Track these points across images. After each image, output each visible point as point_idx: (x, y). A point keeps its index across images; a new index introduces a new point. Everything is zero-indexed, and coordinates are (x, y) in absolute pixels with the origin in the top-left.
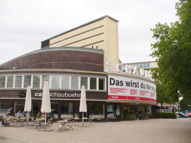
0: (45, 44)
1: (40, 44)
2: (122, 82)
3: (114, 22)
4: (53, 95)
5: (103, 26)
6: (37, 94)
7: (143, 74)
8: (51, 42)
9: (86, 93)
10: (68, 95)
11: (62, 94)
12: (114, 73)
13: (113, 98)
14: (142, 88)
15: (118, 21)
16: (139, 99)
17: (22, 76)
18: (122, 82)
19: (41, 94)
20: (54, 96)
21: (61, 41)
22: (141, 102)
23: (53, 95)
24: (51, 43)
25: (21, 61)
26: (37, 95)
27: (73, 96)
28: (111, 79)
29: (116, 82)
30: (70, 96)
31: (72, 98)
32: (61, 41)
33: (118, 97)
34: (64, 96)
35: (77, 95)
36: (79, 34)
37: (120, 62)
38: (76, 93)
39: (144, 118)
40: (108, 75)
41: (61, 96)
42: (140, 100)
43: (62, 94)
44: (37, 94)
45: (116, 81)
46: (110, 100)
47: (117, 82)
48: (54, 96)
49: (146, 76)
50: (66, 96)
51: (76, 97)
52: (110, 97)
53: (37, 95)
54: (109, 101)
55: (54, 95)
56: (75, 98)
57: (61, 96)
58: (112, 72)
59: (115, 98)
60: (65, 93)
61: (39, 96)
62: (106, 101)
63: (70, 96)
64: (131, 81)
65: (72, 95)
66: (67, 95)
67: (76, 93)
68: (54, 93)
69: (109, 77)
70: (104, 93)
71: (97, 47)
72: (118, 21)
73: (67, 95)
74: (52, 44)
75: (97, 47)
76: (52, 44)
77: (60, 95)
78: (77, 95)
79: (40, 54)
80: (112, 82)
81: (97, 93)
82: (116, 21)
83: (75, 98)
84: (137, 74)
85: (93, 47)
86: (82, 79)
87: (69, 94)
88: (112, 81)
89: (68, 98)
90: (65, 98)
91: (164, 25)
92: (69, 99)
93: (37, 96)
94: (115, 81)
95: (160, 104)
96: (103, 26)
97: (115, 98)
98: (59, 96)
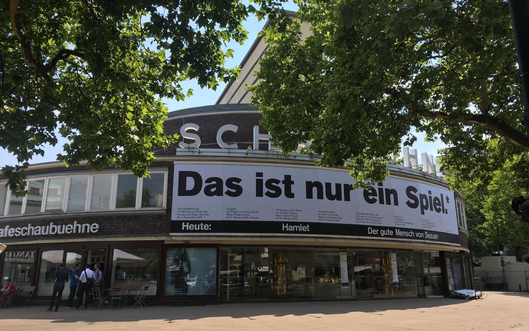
1: (519, 263)
2: (413, 202)
4: (25, 231)
10: (58, 228)
13: (189, 231)
14: (394, 192)
17: (117, 206)
18: (413, 202)
20: (71, 231)
22: (249, 239)
28: (183, 175)
29: (204, 185)
31: (65, 236)
33: (436, 237)
34: (198, 229)
35: (77, 227)
40: (175, 162)
41: (41, 232)
42: (101, 232)
45: (209, 180)
46: (177, 237)
47: (371, 197)
48: (71, 231)
50: (51, 233)
51: (74, 232)
52: (177, 226)
54: (174, 238)
56: (72, 236)
57: (41, 232)
59: (194, 231)
60: (51, 223)
62: (163, 241)
64: (430, 192)
66: (54, 229)
68: (27, 227)
69: (179, 167)
70: (158, 217)
73: (54, 229)
77: (39, 230)
78: (77, 227)
80: (190, 183)
81: (136, 217)
83: (72, 236)
88: (190, 183)
89: (57, 236)
90: (48, 237)
93: (12, 235)
94: (204, 180)
95: (303, 275)
97: (194, 231)
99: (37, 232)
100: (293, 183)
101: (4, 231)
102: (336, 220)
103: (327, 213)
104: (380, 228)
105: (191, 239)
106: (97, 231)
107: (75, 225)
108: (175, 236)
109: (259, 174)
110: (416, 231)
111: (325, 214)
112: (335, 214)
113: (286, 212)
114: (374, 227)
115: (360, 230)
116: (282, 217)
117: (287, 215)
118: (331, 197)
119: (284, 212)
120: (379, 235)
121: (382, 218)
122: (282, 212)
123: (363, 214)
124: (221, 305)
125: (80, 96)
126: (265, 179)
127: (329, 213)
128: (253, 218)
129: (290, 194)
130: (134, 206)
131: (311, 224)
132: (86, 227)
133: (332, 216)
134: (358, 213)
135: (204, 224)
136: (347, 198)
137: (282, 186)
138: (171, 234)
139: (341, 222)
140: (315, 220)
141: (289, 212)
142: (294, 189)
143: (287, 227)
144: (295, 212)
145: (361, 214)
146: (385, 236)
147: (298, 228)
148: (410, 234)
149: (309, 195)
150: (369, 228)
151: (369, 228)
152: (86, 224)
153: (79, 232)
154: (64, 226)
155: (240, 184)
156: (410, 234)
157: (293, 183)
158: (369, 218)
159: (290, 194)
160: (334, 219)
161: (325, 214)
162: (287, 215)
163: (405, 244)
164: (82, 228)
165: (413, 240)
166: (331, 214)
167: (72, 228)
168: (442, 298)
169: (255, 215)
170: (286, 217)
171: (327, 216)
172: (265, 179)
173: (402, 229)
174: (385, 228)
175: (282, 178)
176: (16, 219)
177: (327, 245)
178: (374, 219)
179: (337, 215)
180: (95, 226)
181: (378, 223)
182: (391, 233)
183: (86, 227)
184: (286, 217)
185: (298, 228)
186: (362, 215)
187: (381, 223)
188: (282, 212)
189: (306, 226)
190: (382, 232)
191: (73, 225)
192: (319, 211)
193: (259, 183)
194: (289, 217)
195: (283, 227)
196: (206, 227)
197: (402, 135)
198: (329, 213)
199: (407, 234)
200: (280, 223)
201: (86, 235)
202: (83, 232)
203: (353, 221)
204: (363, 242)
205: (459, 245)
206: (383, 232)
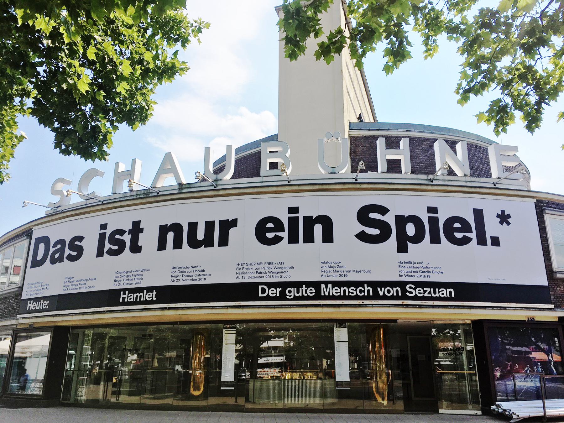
11: (138, 300)
20: (363, 294)
27: (337, 293)
33: (44, 304)
38: (366, 285)
43: (138, 300)
48: (363, 294)
51: (342, 294)
54: (21, 321)
55: (364, 291)
80: (411, 229)
88: (411, 229)
98: (443, 294)
99: (130, 299)
100: (142, 231)
102: (200, 279)
103: (187, 270)
104: (284, 285)
106: (314, 294)
107: (366, 289)
108: (23, 318)
109: (293, 210)
110: (374, 285)
111: (182, 272)
112: (200, 269)
113: (129, 274)
114: (270, 285)
115: (245, 292)
116: (122, 282)
117: (129, 278)
118: (194, 243)
119: (125, 274)
120: (282, 296)
121: (292, 267)
122: (123, 274)
123: (251, 264)
124: (79, 409)
126: (301, 216)
127: (190, 269)
128: (89, 287)
129: (136, 248)
131: (158, 289)
133: (194, 273)
134: (241, 264)
135: (307, 287)
136: (224, 242)
137: (127, 238)
138: (19, 316)
139: (209, 281)
140: (166, 281)
141: (131, 274)
142: (142, 240)
143: (126, 296)
144: (140, 273)
145: (248, 264)
146: (295, 298)
147: (141, 296)
148: (361, 291)
149: (162, 246)
150: (260, 287)
151: (260, 287)
155: (361, 228)
156: (361, 291)
157: (142, 231)
158: (263, 270)
159: (136, 248)
160: (197, 278)
161: (182, 272)
162: (129, 278)
163: (342, 309)
165: (366, 302)
166: (192, 269)
168: (476, 415)
169: (89, 283)
170: (127, 282)
171: (185, 274)
172: (108, 231)
173: (418, 284)
174: (298, 285)
175: (128, 227)
177: (184, 319)
178: (273, 270)
179: (344, 267)
180: (311, 290)
181: (282, 277)
182: (311, 292)
184: (127, 282)
185: (141, 296)
186: (250, 266)
187: (290, 277)
188: (123, 274)
189: (152, 292)
190: (290, 292)
192: (174, 268)
193: (102, 237)
194: (131, 282)
195: (122, 296)
196: (44, 304)
198: (190, 269)
199: (353, 291)
200: (116, 293)
203: (230, 278)
204: (246, 311)
205: (552, 306)
206: (292, 292)
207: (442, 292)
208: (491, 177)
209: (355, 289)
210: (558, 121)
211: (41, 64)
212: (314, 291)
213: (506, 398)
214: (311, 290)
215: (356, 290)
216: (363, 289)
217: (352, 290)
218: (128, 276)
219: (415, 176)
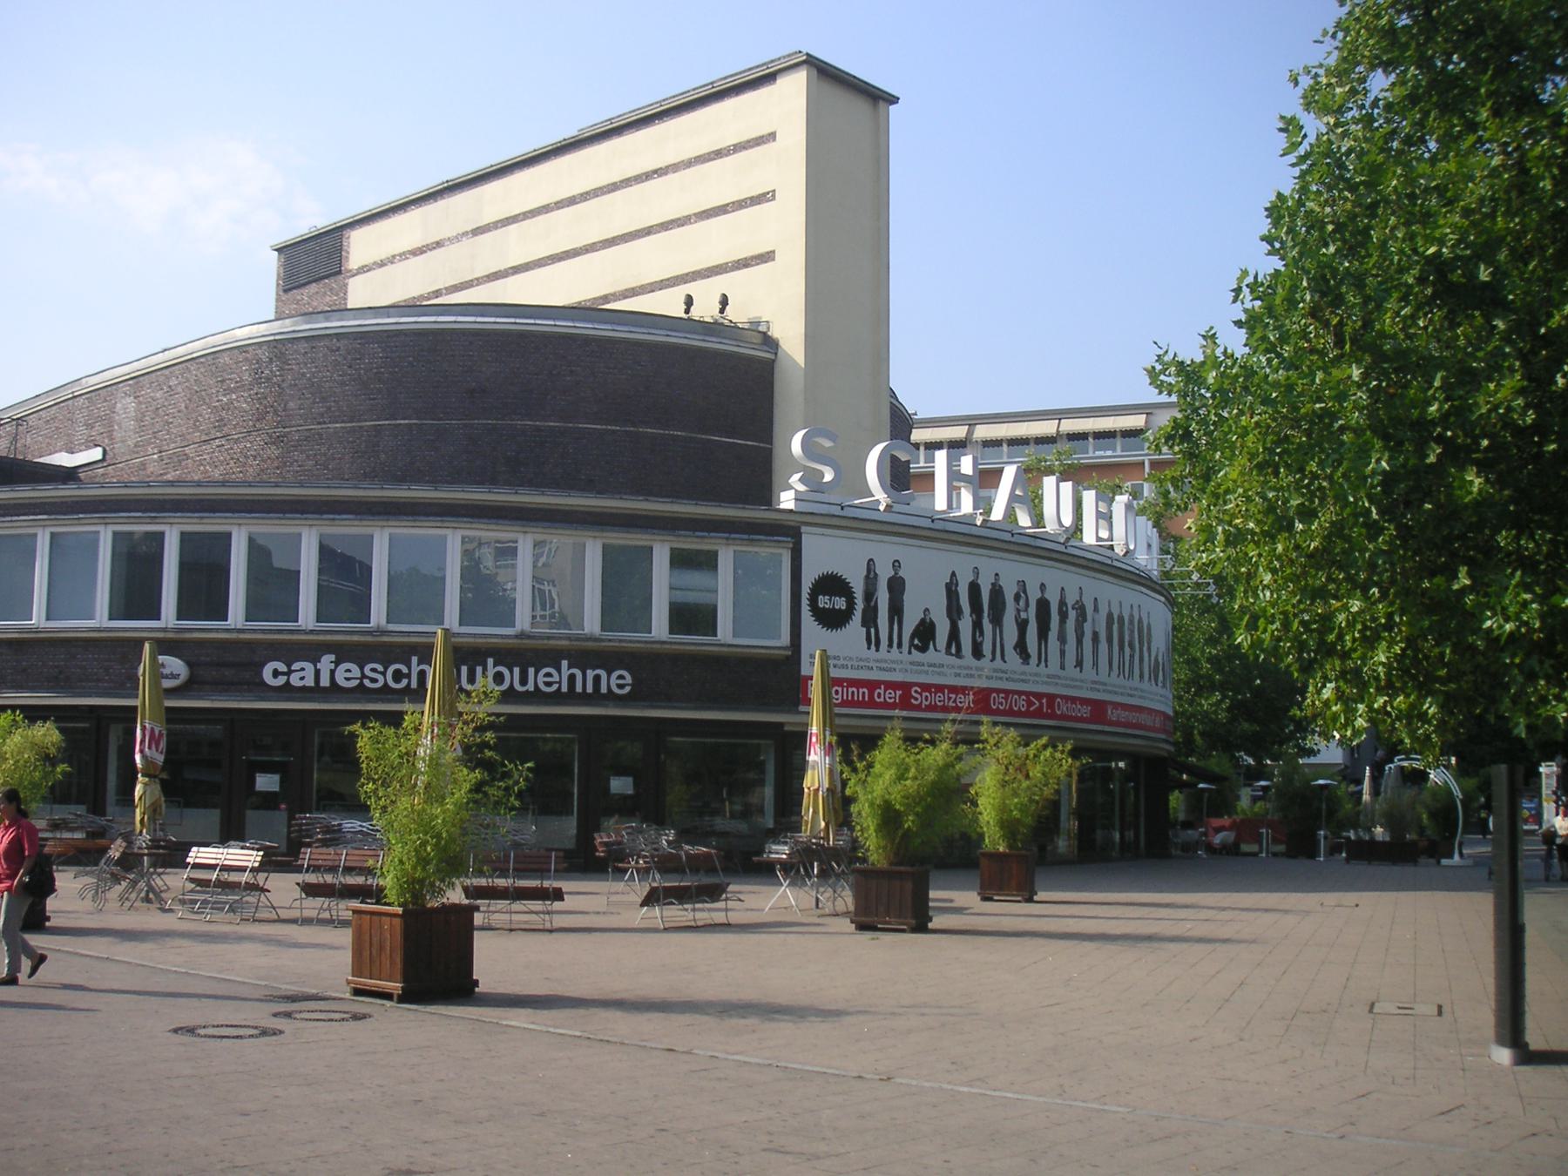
0: (313, 260)
1: (269, 266)
3: (860, 106)
5: (772, 136)
6: (282, 667)
7: (1067, 520)
8: (361, 247)
9: (182, 541)
12: (846, 513)
15: (893, 100)
16: (1085, 711)
19: (309, 666)
20: (555, 687)
21: (439, 244)
23: (398, 676)
24: (355, 258)
25: (126, 406)
26: (276, 673)
27: (548, 684)
30: (524, 682)
31: (537, 696)
32: (439, 244)
35: (572, 678)
36: (585, 196)
37: (901, 423)
38: (565, 663)
39: (126, 406)
40: (803, 529)
44: (282, 667)
48: (405, 682)
49: (1089, 538)
51: (565, 689)
53: (276, 673)
55: (408, 676)
56: (557, 698)
58: (836, 510)
60: (490, 661)
61: (295, 680)
62: (781, 725)
63: (524, 682)
65: (539, 679)
67: (565, 663)
71: (724, 302)
72: (893, 100)
74: (364, 269)
75: (724, 302)
76: (364, 269)
78: (572, 678)
79: (278, 348)
82: (878, 98)
83: (571, 697)
84: (1024, 520)
85: (689, 301)
86: (610, 557)
87: (517, 670)
91: (1300, 91)
92: (515, 703)
93: (281, 680)
96: (772, 136)
101: (317, 673)
105: (854, 722)
106: (628, 689)
107: (566, 672)
125: (1382, 150)
130: (115, 534)
132: (597, 679)
152: (598, 671)
153: (579, 689)
154: (531, 671)
164: (585, 680)
167: (556, 678)
176: (188, 635)
180: (621, 677)
183: (597, 679)
191: (559, 671)
197: (933, 783)
201: (596, 697)
202: (590, 690)
204: (1131, 741)
207: (302, 674)
208: (604, 547)
209: (380, 668)
210: (953, 574)
211: (1464, 591)
212: (629, 679)
213: (909, 886)
214: (621, 677)
215: (384, 674)
216: (405, 670)
217: (373, 670)
218: (1131, 646)
219: (705, 546)
